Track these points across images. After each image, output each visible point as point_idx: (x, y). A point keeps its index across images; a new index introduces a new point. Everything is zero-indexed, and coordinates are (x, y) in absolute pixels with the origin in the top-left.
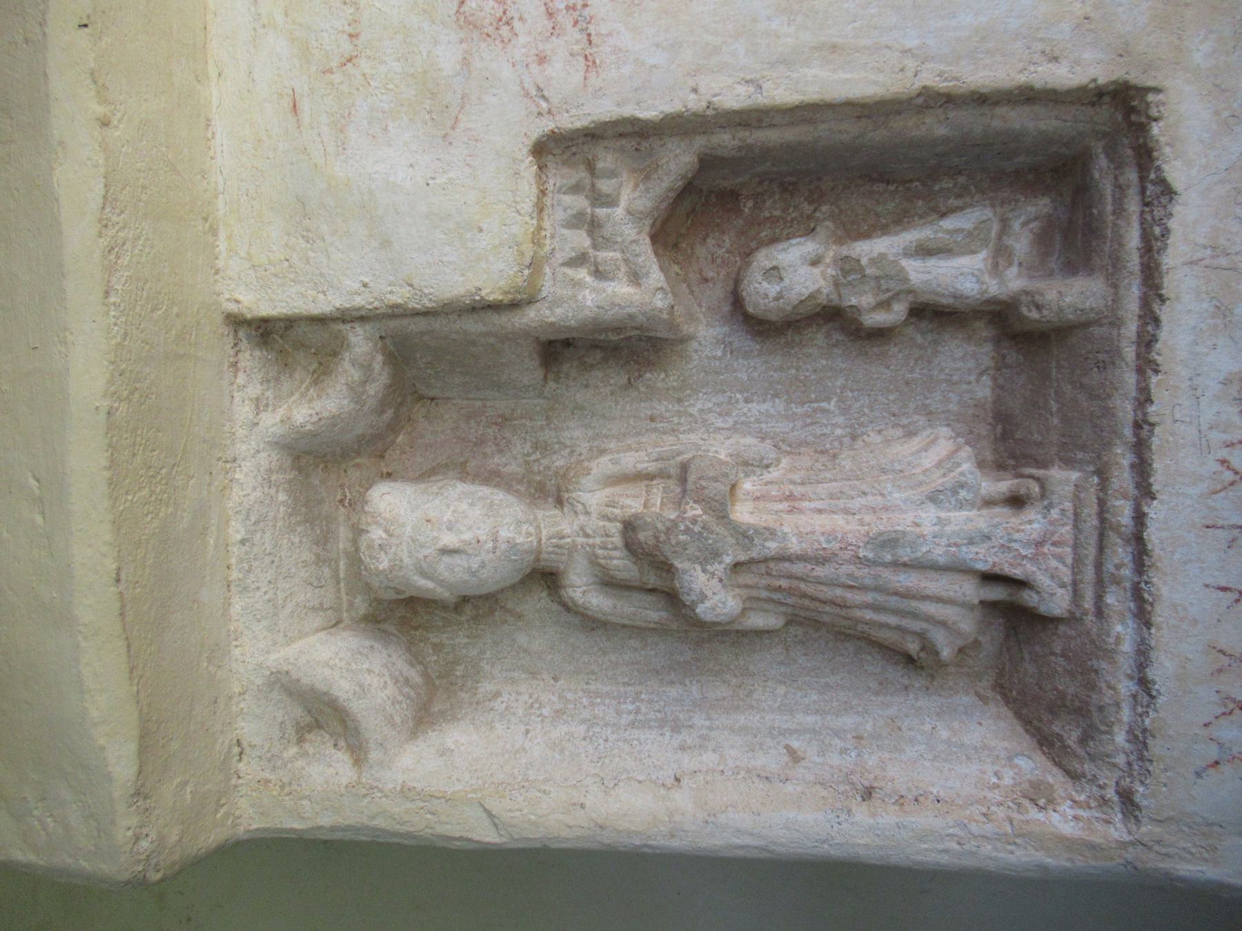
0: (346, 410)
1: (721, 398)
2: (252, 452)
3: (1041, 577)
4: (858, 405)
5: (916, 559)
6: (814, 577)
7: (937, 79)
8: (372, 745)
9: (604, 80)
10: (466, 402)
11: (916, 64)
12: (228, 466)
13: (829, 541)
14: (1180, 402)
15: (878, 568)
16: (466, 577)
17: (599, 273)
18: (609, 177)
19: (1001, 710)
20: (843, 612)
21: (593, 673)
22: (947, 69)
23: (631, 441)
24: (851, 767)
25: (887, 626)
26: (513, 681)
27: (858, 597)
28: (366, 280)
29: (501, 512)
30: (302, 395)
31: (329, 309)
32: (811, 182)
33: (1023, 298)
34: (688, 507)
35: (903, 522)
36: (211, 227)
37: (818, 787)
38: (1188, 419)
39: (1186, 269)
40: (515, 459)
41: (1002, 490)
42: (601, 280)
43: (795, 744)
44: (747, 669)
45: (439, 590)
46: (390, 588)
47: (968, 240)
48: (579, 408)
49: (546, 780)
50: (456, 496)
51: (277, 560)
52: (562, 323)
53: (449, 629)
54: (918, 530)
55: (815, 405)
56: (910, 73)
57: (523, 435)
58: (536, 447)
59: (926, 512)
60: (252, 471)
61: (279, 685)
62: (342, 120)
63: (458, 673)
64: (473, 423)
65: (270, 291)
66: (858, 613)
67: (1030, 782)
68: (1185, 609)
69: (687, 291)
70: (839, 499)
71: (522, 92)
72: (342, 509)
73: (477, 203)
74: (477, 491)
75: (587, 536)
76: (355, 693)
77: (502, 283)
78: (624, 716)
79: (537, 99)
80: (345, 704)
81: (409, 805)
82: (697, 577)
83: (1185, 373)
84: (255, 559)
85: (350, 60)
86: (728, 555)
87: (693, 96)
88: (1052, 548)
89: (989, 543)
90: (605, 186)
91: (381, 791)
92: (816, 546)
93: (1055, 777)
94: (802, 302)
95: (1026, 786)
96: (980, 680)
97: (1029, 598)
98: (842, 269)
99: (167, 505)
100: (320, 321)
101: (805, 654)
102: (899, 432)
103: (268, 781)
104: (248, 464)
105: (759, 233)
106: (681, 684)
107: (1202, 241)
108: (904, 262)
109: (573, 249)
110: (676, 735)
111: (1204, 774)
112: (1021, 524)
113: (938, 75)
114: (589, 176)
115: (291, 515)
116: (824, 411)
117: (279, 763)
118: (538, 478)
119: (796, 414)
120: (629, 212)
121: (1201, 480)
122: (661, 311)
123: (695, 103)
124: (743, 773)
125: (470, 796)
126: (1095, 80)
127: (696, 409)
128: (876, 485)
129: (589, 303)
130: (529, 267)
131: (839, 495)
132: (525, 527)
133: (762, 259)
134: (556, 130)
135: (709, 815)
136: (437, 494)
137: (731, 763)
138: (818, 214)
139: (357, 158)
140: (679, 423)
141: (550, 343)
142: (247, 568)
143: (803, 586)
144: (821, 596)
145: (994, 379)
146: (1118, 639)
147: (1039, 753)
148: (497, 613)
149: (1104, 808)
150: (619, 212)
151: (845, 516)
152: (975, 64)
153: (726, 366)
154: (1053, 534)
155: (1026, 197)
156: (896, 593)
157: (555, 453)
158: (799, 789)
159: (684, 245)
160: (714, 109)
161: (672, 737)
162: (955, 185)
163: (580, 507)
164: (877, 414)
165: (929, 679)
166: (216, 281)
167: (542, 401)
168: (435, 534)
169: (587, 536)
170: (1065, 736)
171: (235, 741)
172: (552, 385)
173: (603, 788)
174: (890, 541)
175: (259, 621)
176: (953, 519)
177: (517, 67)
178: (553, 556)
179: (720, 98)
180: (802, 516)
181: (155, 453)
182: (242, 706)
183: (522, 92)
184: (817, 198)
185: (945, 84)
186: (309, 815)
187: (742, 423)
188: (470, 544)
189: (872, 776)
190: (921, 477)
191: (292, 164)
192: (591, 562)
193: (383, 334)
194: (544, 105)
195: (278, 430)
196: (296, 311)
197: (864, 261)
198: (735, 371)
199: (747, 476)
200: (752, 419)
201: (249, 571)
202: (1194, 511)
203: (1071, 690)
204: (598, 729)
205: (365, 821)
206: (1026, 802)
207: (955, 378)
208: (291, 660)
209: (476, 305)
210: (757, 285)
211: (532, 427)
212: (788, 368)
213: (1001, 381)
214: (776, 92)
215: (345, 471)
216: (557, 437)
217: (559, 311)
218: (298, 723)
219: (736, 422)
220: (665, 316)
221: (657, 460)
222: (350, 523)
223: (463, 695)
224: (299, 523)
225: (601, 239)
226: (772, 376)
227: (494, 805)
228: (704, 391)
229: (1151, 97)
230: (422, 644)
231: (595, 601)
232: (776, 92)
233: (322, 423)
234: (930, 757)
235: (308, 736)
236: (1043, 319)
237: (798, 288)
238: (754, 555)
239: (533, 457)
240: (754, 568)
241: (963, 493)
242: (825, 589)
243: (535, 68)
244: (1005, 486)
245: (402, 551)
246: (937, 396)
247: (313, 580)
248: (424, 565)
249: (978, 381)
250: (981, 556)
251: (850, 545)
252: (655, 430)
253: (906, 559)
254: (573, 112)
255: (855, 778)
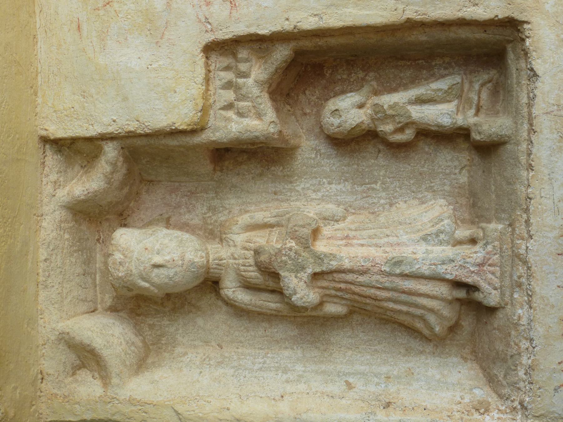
0: (103, 187)
1: (314, 181)
2: (51, 211)
3: (483, 284)
4: (393, 186)
5: (413, 272)
6: (358, 282)
7: (415, 14)
8: (113, 375)
9: (240, 14)
10: (169, 183)
11: (403, 6)
12: (39, 218)
13: (365, 262)
14: (544, 187)
15: (393, 277)
16: (167, 281)
17: (241, 114)
18: (245, 62)
19: (474, 365)
20: (377, 303)
21: (241, 342)
22: (419, 9)
23: (263, 206)
24: (380, 392)
25: (400, 312)
26: (195, 347)
27: (383, 294)
28: (115, 118)
29: (187, 245)
30: (78, 180)
31: (95, 134)
32: (363, 60)
33: (473, 128)
34: (287, 241)
35: (407, 252)
36: (34, 92)
37: (360, 402)
38: (548, 196)
39: (545, 117)
40: (198, 216)
41: (466, 235)
42: (240, 117)
43: (351, 380)
44: (330, 340)
45: (152, 288)
46: (125, 287)
47: (445, 95)
48: (234, 186)
49: (209, 396)
50: (162, 236)
51: (63, 270)
52: (219, 141)
53: (159, 316)
54: (414, 256)
55: (368, 186)
56: (400, 11)
57: (202, 202)
58: (209, 209)
59: (421, 246)
60: (51, 221)
61: (63, 341)
62: (103, 34)
63: (163, 342)
64: (174, 196)
65: (63, 124)
66: (386, 304)
67: (479, 401)
68: (548, 299)
69: (295, 120)
70: (374, 238)
71: (198, 20)
72: (98, 245)
73: (174, 78)
74: (174, 234)
75: (235, 259)
76: (105, 345)
77: (186, 120)
78: (257, 365)
79: (205, 24)
80: (99, 351)
81: (133, 408)
82: (292, 280)
83: (546, 172)
84: (52, 270)
85: (108, 4)
86: (309, 268)
87: (287, 22)
88: (489, 267)
89: (454, 264)
90: (243, 67)
91: (118, 400)
92: (358, 264)
93: (493, 399)
94: (352, 129)
95: (475, 403)
96: (464, 349)
97: (479, 296)
98: (374, 111)
99: (11, 239)
100: (90, 139)
101: (363, 332)
102: (416, 202)
103: (56, 395)
104: (49, 218)
105: (334, 88)
106: (291, 349)
107: (552, 102)
108: (410, 108)
109: (225, 101)
110: (284, 375)
111: (559, 390)
112: (471, 253)
113: (416, 12)
114: (234, 61)
115: (71, 246)
116: (373, 189)
117: (63, 385)
118: (210, 227)
119: (357, 191)
120: (256, 81)
121: (555, 229)
122: (273, 134)
123: (288, 26)
124: (319, 394)
125: (166, 403)
126: (497, 16)
127: (301, 188)
128: (394, 231)
129: (234, 130)
130: (200, 111)
131: (374, 236)
132: (200, 253)
133: (331, 105)
134: (215, 40)
135: (297, 414)
136: (151, 234)
137: (314, 390)
138: (367, 78)
139: (111, 54)
140: (290, 196)
141: (217, 150)
142: (47, 275)
143: (353, 287)
144: (362, 293)
145: (469, 171)
146: (520, 318)
147: (488, 386)
148: (186, 307)
149: (513, 413)
150: (250, 81)
151: (375, 248)
152: (434, 7)
153: (317, 164)
154: (489, 259)
155: (483, 70)
156: (404, 292)
157: (220, 212)
158: (349, 402)
159: (293, 94)
160: (298, 29)
161: (282, 375)
162: (444, 62)
163: (231, 243)
164: (404, 191)
165: (435, 347)
166: (36, 119)
167: (213, 183)
168: (150, 256)
169: (235, 259)
170: (499, 375)
171: (39, 371)
172: (219, 173)
173: (240, 400)
174: (398, 263)
175: (53, 304)
176: (434, 251)
177: (195, 7)
178: (216, 270)
179: (301, 23)
180: (353, 248)
181: (7, 211)
182: (44, 351)
183: (198, 20)
184: (366, 68)
185: (419, 17)
186: (79, 413)
187: (327, 196)
188: (169, 262)
189: (391, 397)
190: (420, 227)
191: (77, 57)
192: (237, 274)
193: (123, 146)
194: (209, 27)
195: (66, 199)
196: (77, 135)
197: (386, 107)
198: (322, 166)
199: (325, 226)
200: (332, 194)
201: (49, 276)
202: (551, 246)
203: (501, 349)
204: (240, 371)
205: (109, 417)
206: (473, 411)
207: (448, 171)
208: (70, 327)
209: (173, 131)
210: (328, 119)
211: (207, 198)
212: (353, 165)
213: (472, 173)
214: (330, 21)
215: (100, 223)
216: (221, 204)
217: (217, 134)
218: (73, 364)
219: (323, 196)
220: (276, 136)
221: (275, 217)
222: (103, 253)
223: (166, 355)
224: (75, 251)
225: (240, 95)
226: (343, 169)
227: (180, 408)
228: (305, 177)
229: (526, 26)
230: (142, 325)
231: (240, 297)
232: (330, 21)
233: (90, 195)
234: (426, 388)
235: (78, 372)
236: (482, 140)
237: (350, 121)
238: (324, 269)
239: (208, 215)
240: (326, 277)
241: (442, 236)
242: (365, 289)
243: (204, 8)
244: (463, 233)
245: (132, 265)
246: (438, 181)
247: (82, 284)
248: (144, 274)
249: (460, 173)
250: (449, 271)
251: (377, 264)
252: (277, 200)
253: (407, 272)
254: (224, 30)
255: (381, 398)
